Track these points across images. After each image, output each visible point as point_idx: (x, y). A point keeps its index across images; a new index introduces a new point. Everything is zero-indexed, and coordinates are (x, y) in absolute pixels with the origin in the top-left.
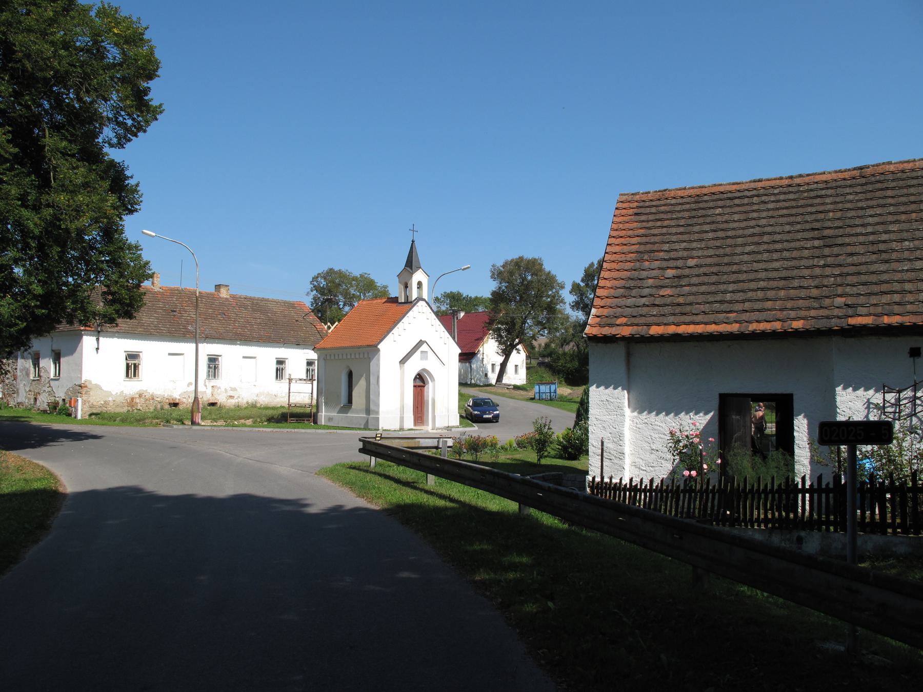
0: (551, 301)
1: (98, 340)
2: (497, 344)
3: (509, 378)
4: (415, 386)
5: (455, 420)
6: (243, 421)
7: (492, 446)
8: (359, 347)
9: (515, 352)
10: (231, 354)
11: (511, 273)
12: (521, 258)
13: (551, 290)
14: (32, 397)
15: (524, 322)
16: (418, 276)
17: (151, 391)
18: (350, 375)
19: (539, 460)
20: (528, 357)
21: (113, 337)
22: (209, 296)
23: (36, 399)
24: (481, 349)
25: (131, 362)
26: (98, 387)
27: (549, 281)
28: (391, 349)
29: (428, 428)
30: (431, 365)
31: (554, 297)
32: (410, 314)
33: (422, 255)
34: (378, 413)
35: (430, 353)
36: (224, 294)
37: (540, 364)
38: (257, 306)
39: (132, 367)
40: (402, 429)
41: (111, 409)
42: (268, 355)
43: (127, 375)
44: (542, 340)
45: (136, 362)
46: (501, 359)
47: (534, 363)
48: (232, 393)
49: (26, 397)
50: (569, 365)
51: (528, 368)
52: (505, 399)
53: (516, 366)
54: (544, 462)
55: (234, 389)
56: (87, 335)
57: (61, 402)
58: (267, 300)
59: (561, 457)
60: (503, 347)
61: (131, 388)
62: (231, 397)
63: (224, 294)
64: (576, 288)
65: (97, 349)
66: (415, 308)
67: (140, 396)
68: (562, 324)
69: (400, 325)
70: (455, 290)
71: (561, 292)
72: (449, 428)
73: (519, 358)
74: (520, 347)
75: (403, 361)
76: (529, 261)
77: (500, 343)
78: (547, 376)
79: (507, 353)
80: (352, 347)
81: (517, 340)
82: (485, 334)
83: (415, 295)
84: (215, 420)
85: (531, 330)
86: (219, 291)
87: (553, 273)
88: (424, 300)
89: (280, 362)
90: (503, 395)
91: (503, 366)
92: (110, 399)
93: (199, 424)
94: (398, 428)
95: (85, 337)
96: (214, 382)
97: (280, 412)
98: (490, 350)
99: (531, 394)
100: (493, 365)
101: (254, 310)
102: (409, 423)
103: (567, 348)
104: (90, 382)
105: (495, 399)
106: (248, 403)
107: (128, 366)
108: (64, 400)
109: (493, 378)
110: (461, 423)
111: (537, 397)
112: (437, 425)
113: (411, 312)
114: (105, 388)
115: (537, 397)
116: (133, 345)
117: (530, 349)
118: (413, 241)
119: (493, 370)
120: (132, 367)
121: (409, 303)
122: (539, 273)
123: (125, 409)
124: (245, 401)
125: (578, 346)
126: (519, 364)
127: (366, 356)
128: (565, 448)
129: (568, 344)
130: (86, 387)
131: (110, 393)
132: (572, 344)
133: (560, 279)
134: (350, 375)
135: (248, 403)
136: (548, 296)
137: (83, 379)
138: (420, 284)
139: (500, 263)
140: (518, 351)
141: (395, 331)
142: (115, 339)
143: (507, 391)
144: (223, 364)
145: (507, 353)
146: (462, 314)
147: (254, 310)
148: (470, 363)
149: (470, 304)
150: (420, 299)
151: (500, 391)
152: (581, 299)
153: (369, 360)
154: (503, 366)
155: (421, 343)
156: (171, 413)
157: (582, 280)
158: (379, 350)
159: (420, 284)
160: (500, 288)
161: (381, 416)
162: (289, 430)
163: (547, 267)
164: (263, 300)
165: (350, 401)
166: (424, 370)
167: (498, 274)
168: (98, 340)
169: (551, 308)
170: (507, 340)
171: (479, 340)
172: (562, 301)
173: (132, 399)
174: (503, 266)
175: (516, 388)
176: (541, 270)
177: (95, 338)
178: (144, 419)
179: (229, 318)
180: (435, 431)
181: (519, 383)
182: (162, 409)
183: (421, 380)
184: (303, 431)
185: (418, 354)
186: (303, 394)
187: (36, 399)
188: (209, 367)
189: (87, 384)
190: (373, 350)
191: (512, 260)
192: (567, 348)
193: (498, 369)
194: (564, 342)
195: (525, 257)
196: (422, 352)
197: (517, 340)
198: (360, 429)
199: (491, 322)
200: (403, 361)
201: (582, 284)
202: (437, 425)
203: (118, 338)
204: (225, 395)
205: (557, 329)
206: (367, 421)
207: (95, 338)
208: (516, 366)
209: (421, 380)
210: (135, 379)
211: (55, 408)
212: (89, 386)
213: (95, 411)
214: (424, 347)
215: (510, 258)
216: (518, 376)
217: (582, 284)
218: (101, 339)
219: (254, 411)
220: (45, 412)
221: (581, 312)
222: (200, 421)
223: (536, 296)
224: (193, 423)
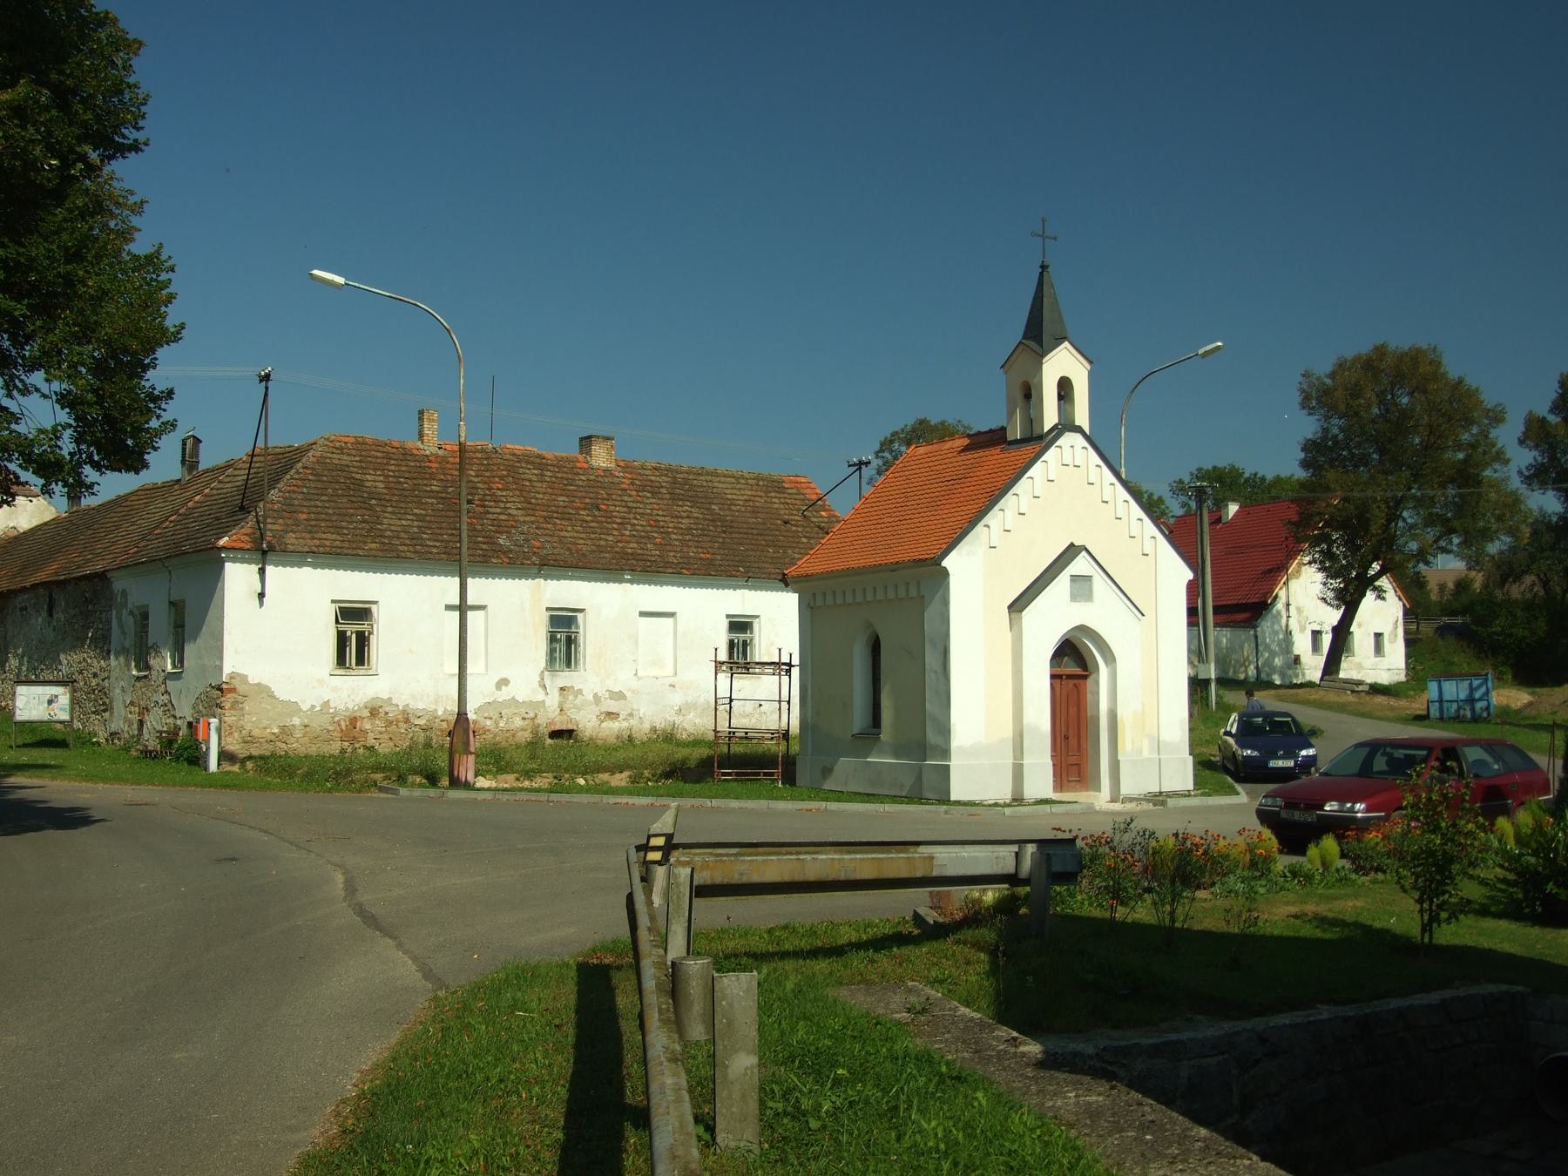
0: (1466, 461)
1: (262, 572)
2: (1320, 576)
3: (1360, 667)
4: (1053, 677)
5: (1179, 774)
6: (605, 777)
7: (1253, 864)
8: (895, 567)
9: (1370, 596)
10: (606, 603)
11: (1355, 392)
12: (1381, 351)
13: (1466, 428)
14: (135, 718)
15: (1393, 517)
16: (1063, 363)
17: (402, 700)
18: (875, 647)
19: (1426, 928)
20: (1411, 614)
21: (300, 565)
22: (561, 464)
23: (141, 723)
24: (1282, 594)
25: (351, 629)
26: (263, 690)
27: (1461, 408)
28: (978, 574)
29: (1101, 799)
30: (1103, 615)
31: (1474, 446)
32: (1036, 470)
33: (1066, 297)
34: (945, 752)
35: (1100, 582)
36: (601, 457)
37: (1442, 631)
38: (683, 487)
39: (353, 638)
40: (1018, 800)
41: (298, 745)
42: (705, 609)
43: (341, 660)
44: (1447, 567)
45: (364, 627)
46: (1334, 616)
47: (1427, 629)
48: (613, 706)
49: (126, 720)
50: (1520, 632)
51: (1410, 642)
52: (1344, 717)
53: (1378, 636)
54: (1449, 934)
55: (620, 696)
56: (234, 560)
57: (183, 732)
58: (714, 474)
59: (1514, 912)
60: (1336, 583)
61: (352, 692)
62: (611, 715)
63: (601, 457)
64: (1536, 432)
65: (261, 595)
66: (1051, 455)
67: (374, 712)
68: (1500, 518)
69: (1009, 501)
70: (1222, 463)
71: (1493, 433)
72: (1159, 798)
73: (1382, 613)
74: (1384, 582)
75: (1018, 606)
76: (1401, 357)
77: (1330, 573)
78: (1462, 660)
79: (1349, 601)
80: (876, 569)
81: (1376, 567)
82: (1291, 555)
83: (1050, 418)
84: (528, 774)
85: (1414, 537)
86: (589, 453)
87: (1472, 381)
88: (1079, 430)
89: (740, 625)
90: (1341, 708)
91: (1342, 633)
92: (296, 721)
93: (467, 786)
94: (1004, 793)
95: (228, 565)
96: (566, 678)
97: (705, 752)
98: (1305, 597)
99: (1418, 707)
100: (1316, 635)
101: (674, 497)
102: (1040, 781)
103: (1516, 591)
104: (244, 678)
105: (1306, 716)
106: (654, 730)
107: (342, 639)
108: (190, 724)
109: (1313, 667)
110: (1198, 782)
111: (1434, 711)
112: (1126, 789)
113: (1038, 466)
114: (282, 693)
115: (1434, 711)
116: (356, 584)
117: (1412, 590)
118: (1044, 267)
119: (1316, 646)
120: (353, 638)
121: (1038, 441)
122: (1432, 387)
123: (335, 748)
124: (647, 726)
125: (1545, 584)
126: (1386, 630)
127: (913, 593)
128: (1529, 880)
129: (1518, 578)
130: (233, 690)
131: (293, 707)
132: (1529, 579)
133: (1489, 398)
134: (875, 647)
135: (654, 730)
136: (1459, 446)
137: (227, 669)
138: (1065, 387)
139: (1323, 367)
140: (1380, 595)
141: (994, 518)
142: (307, 570)
143: (1351, 698)
144: (590, 635)
145: (1349, 601)
146: (1233, 508)
147: (674, 497)
148: (1255, 627)
149: (1254, 491)
150: (1066, 425)
151: (1332, 697)
152: (1553, 458)
153: (921, 603)
154: (1342, 633)
155: (1071, 552)
156: (441, 756)
157: (1555, 409)
158: (945, 574)
159: (1065, 387)
160: (1325, 430)
161: (955, 763)
162: (697, 802)
163: (1453, 368)
164: (702, 472)
165: (876, 721)
166: (1083, 629)
167: (1317, 397)
168: (262, 572)
169: (1466, 476)
170: (1350, 566)
171: (1276, 571)
172: (1500, 458)
173: (353, 721)
174: (1332, 375)
175: (1376, 689)
176: (1437, 375)
177: (255, 568)
178: (349, 772)
179: (609, 516)
180: (1117, 807)
181: (1384, 679)
182: (428, 745)
183: (1074, 660)
184: (734, 804)
185: (1062, 583)
186: (767, 705)
187: (141, 723)
188: (553, 639)
189: (236, 683)
190: (926, 580)
191: (1356, 359)
192: (1516, 591)
193: (1327, 640)
194: (1507, 571)
195: (1392, 346)
196: (1074, 578)
197: (1376, 567)
198: (895, 799)
199: (1305, 521)
200: (1018, 606)
201: (1553, 419)
202: (1126, 789)
203: (315, 566)
204: (596, 710)
205: (1486, 535)
206: (919, 777)
207: (255, 568)
208: (1378, 636)
209: (1074, 660)
210: (362, 670)
211: (171, 742)
212: (241, 688)
213: (255, 752)
214: (1080, 565)
215: (1349, 354)
216: (1384, 662)
217: (1553, 419)
218: (270, 569)
219: (632, 753)
220: (147, 754)
221: (1551, 494)
222: (470, 777)
223: (1426, 447)
224: (455, 782)
